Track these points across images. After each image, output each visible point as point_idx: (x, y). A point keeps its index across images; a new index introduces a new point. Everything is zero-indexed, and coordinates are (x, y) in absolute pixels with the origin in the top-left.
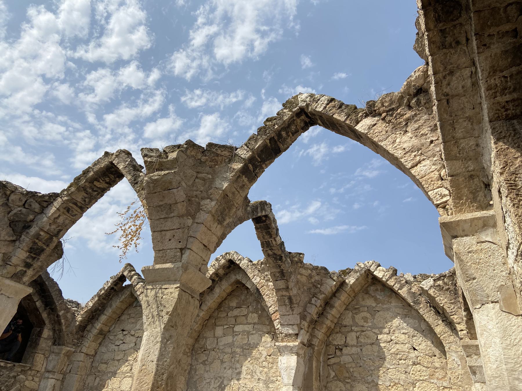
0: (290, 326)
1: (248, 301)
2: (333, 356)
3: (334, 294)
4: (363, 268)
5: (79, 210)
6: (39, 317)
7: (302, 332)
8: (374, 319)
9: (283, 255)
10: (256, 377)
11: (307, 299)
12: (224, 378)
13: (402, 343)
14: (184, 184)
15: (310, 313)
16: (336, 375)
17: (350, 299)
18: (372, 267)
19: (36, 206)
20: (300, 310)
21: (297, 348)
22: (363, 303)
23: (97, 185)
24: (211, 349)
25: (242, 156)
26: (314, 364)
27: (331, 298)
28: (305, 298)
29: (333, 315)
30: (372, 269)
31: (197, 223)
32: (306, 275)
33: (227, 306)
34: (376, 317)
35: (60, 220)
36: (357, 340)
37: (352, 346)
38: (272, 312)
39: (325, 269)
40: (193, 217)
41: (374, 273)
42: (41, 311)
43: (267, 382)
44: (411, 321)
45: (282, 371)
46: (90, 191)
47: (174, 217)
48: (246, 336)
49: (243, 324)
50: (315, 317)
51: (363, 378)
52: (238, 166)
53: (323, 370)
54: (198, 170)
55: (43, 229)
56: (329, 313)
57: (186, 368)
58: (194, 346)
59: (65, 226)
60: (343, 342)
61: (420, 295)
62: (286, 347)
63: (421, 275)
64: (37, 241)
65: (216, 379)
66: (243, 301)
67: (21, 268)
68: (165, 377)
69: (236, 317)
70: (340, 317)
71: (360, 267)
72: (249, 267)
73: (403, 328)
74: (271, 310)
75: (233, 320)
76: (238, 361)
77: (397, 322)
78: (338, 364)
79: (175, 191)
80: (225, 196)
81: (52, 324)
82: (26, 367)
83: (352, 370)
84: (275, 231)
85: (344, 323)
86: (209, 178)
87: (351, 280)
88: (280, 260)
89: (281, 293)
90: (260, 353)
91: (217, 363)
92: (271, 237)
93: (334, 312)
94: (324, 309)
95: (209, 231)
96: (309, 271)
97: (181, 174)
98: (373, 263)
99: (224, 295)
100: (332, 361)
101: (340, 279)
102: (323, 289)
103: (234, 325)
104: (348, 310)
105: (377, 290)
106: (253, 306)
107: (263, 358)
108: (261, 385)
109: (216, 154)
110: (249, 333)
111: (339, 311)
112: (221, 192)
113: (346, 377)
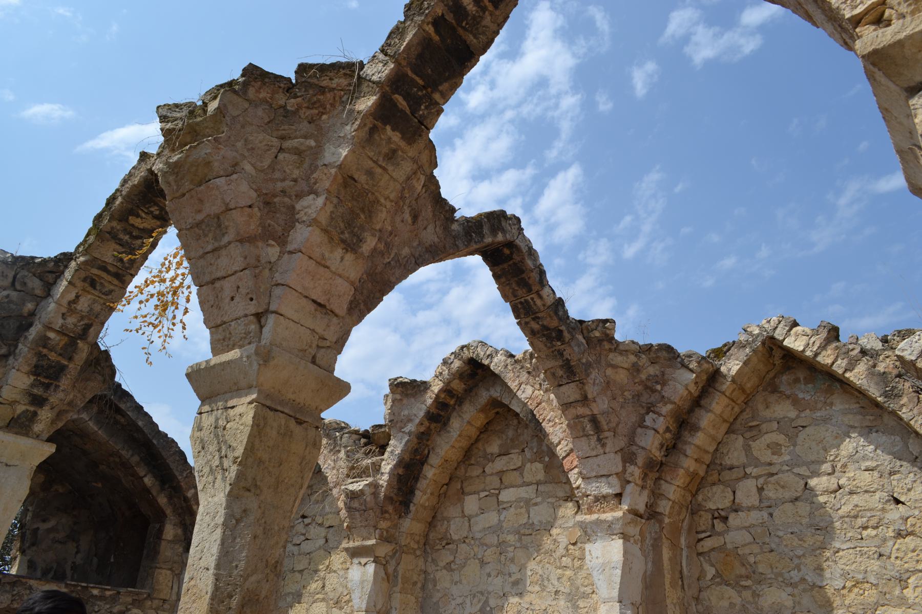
0: (604, 479)
1: (521, 439)
2: (708, 534)
3: (697, 402)
4: (758, 335)
5: (116, 282)
6: (153, 503)
7: (629, 488)
8: (795, 445)
9: (563, 328)
10: (550, 588)
11: (634, 418)
12: (489, 593)
13: (866, 491)
14: (248, 167)
15: (643, 448)
16: (718, 574)
17: (737, 409)
18: (777, 331)
19: (35, 284)
20: (622, 442)
21: (621, 522)
22: (767, 414)
23: (137, 225)
24: (459, 540)
25: (375, 78)
26: (666, 554)
27: (691, 411)
28: (628, 417)
29: (698, 447)
30: (779, 335)
31: (290, 253)
32: (626, 366)
33: (481, 454)
34: (800, 440)
35: (83, 305)
36: (760, 495)
37: (749, 509)
38: (564, 454)
39: (668, 349)
40: (282, 241)
41: (785, 343)
42: (154, 493)
43: (574, 597)
44: (883, 438)
45: (595, 574)
46: (127, 237)
47: (229, 243)
48: (523, 510)
49: (516, 486)
50: (658, 455)
51: (781, 574)
52: (366, 103)
53: (688, 564)
54: (280, 133)
55: (53, 326)
56: (690, 443)
57: (415, 579)
58: (427, 536)
59: (96, 317)
60: (727, 503)
61: (899, 376)
62: (598, 522)
63: (899, 332)
64: (45, 351)
65: (474, 597)
66: (512, 440)
67: (24, 408)
68: (235, 602)
69: (500, 474)
70: (717, 450)
71: (751, 334)
72: (510, 367)
73: (865, 458)
74: (561, 450)
75: (496, 479)
76: (512, 560)
77: (848, 446)
78: (722, 549)
79: (221, 181)
80: (347, 180)
81: (179, 515)
82: (141, 594)
83: (752, 559)
84: (535, 276)
85: (728, 462)
86: (311, 148)
87: (732, 366)
88: (559, 340)
89: (572, 412)
90: (555, 540)
91: (473, 568)
92: (530, 291)
93: (699, 439)
94: (678, 437)
95: (322, 269)
96: (632, 358)
97: (239, 145)
98: (780, 322)
99: (473, 432)
100: (708, 544)
101: (706, 366)
102: (667, 392)
103: (499, 489)
104: (733, 432)
105: (797, 380)
106: (532, 449)
107: (561, 550)
108: (562, 603)
109: (323, 84)
110: (528, 503)
111: (713, 438)
112: (333, 171)
113: (741, 576)
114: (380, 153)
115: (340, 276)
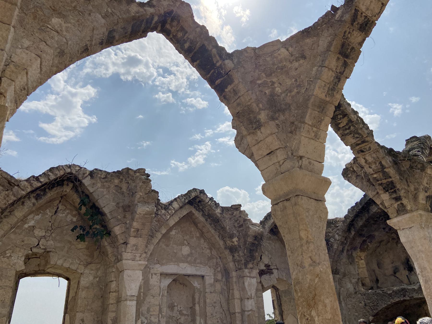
23: (343, 125)
46: (348, 131)
64: (380, 182)
95: (260, 144)
114: (233, 97)
115: (266, 137)
